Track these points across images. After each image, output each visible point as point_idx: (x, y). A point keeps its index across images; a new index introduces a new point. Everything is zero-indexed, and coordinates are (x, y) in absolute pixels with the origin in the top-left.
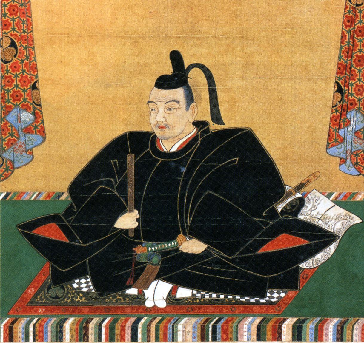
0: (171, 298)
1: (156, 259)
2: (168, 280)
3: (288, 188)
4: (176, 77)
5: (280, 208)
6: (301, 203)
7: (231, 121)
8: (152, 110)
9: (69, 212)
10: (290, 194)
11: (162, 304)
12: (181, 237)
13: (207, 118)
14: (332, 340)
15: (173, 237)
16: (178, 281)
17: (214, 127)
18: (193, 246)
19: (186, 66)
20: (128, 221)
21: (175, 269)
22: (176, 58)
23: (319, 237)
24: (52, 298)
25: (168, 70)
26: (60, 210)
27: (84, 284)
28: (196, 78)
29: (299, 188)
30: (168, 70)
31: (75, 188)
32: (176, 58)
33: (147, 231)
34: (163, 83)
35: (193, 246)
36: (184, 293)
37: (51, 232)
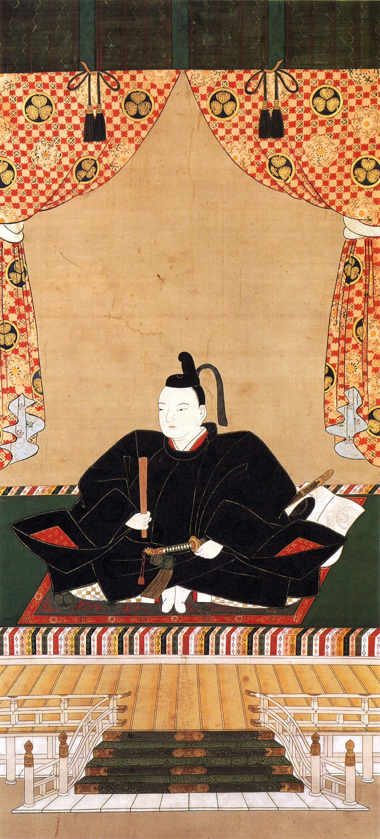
0: (190, 602)
1: (170, 563)
2: (186, 586)
3: (298, 489)
4: (188, 376)
5: (289, 510)
6: (310, 503)
7: (235, 425)
8: (161, 410)
9: (78, 510)
10: (300, 495)
11: (181, 609)
12: (193, 539)
13: (215, 420)
14: (318, 654)
15: (186, 541)
16: (195, 586)
17: (221, 430)
18: (210, 550)
19: (197, 366)
20: (140, 521)
21: (191, 573)
22: (185, 358)
23: (328, 539)
24: (373, 434)
25: (178, 369)
26: (68, 507)
27: (92, 592)
28: (206, 379)
29: (308, 490)
30: (178, 369)
31: (84, 482)
32: (185, 358)
33: (158, 533)
34: (174, 382)
35: (210, 550)
36: (203, 598)
37: (54, 536)
